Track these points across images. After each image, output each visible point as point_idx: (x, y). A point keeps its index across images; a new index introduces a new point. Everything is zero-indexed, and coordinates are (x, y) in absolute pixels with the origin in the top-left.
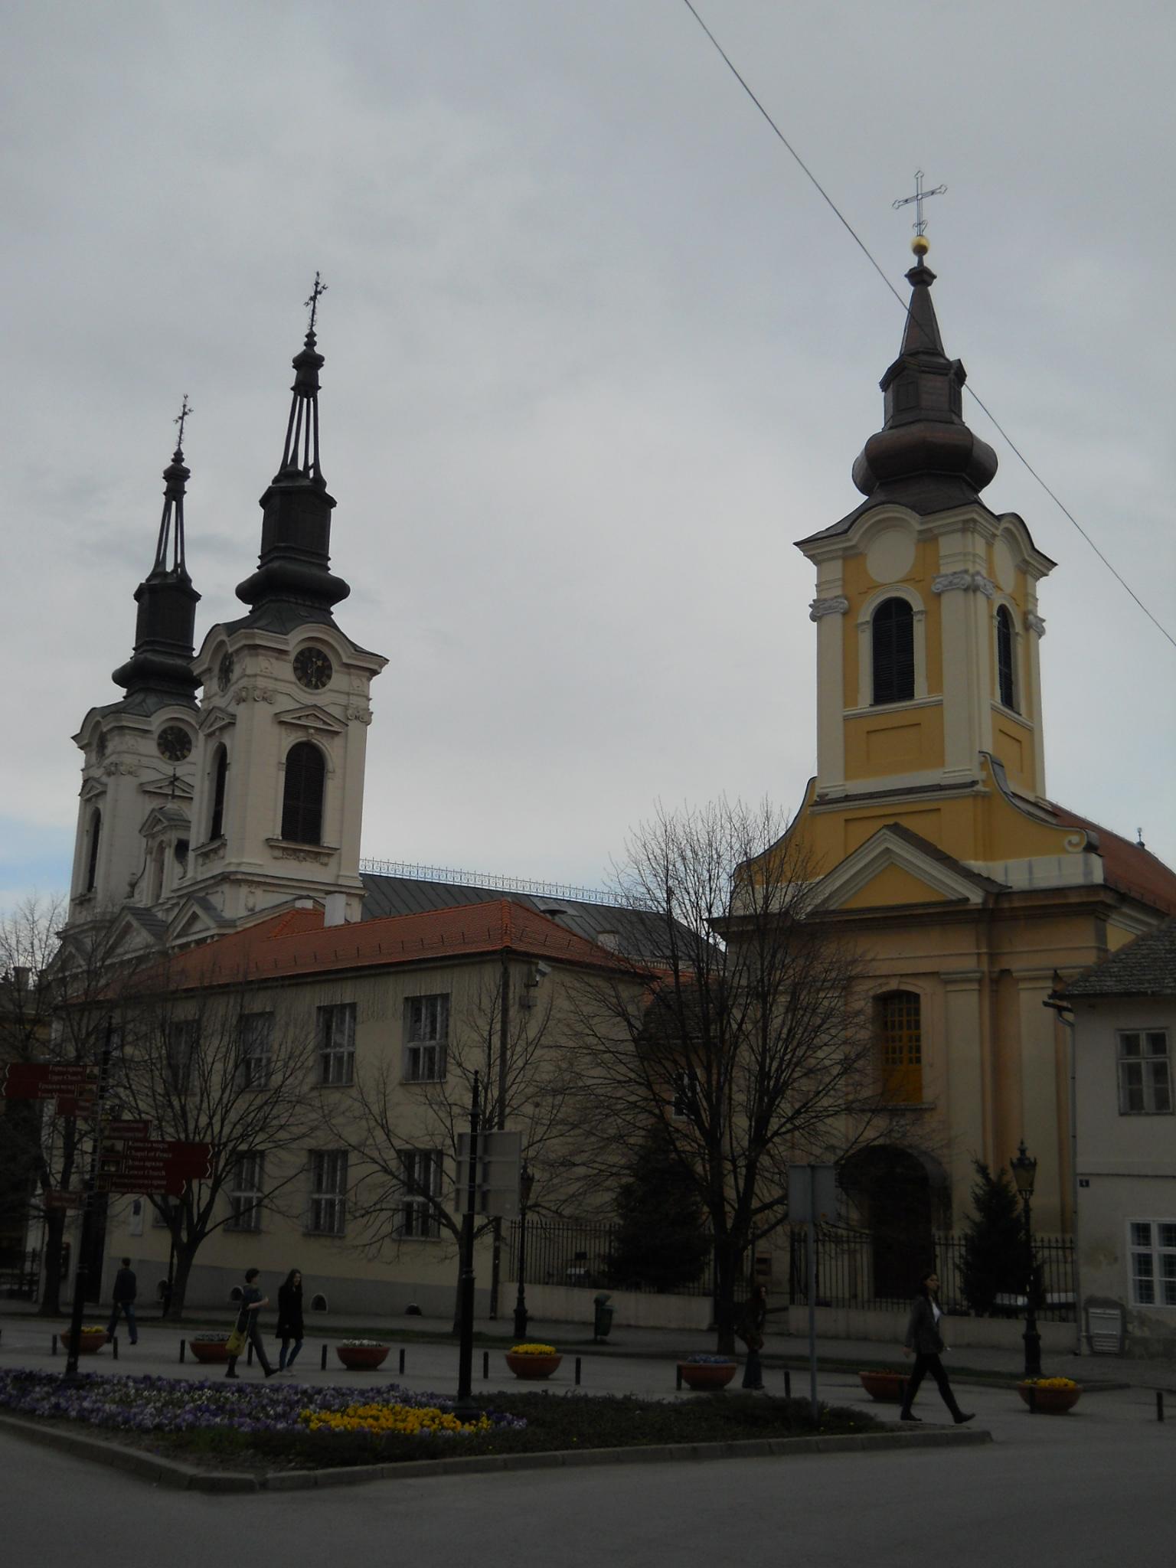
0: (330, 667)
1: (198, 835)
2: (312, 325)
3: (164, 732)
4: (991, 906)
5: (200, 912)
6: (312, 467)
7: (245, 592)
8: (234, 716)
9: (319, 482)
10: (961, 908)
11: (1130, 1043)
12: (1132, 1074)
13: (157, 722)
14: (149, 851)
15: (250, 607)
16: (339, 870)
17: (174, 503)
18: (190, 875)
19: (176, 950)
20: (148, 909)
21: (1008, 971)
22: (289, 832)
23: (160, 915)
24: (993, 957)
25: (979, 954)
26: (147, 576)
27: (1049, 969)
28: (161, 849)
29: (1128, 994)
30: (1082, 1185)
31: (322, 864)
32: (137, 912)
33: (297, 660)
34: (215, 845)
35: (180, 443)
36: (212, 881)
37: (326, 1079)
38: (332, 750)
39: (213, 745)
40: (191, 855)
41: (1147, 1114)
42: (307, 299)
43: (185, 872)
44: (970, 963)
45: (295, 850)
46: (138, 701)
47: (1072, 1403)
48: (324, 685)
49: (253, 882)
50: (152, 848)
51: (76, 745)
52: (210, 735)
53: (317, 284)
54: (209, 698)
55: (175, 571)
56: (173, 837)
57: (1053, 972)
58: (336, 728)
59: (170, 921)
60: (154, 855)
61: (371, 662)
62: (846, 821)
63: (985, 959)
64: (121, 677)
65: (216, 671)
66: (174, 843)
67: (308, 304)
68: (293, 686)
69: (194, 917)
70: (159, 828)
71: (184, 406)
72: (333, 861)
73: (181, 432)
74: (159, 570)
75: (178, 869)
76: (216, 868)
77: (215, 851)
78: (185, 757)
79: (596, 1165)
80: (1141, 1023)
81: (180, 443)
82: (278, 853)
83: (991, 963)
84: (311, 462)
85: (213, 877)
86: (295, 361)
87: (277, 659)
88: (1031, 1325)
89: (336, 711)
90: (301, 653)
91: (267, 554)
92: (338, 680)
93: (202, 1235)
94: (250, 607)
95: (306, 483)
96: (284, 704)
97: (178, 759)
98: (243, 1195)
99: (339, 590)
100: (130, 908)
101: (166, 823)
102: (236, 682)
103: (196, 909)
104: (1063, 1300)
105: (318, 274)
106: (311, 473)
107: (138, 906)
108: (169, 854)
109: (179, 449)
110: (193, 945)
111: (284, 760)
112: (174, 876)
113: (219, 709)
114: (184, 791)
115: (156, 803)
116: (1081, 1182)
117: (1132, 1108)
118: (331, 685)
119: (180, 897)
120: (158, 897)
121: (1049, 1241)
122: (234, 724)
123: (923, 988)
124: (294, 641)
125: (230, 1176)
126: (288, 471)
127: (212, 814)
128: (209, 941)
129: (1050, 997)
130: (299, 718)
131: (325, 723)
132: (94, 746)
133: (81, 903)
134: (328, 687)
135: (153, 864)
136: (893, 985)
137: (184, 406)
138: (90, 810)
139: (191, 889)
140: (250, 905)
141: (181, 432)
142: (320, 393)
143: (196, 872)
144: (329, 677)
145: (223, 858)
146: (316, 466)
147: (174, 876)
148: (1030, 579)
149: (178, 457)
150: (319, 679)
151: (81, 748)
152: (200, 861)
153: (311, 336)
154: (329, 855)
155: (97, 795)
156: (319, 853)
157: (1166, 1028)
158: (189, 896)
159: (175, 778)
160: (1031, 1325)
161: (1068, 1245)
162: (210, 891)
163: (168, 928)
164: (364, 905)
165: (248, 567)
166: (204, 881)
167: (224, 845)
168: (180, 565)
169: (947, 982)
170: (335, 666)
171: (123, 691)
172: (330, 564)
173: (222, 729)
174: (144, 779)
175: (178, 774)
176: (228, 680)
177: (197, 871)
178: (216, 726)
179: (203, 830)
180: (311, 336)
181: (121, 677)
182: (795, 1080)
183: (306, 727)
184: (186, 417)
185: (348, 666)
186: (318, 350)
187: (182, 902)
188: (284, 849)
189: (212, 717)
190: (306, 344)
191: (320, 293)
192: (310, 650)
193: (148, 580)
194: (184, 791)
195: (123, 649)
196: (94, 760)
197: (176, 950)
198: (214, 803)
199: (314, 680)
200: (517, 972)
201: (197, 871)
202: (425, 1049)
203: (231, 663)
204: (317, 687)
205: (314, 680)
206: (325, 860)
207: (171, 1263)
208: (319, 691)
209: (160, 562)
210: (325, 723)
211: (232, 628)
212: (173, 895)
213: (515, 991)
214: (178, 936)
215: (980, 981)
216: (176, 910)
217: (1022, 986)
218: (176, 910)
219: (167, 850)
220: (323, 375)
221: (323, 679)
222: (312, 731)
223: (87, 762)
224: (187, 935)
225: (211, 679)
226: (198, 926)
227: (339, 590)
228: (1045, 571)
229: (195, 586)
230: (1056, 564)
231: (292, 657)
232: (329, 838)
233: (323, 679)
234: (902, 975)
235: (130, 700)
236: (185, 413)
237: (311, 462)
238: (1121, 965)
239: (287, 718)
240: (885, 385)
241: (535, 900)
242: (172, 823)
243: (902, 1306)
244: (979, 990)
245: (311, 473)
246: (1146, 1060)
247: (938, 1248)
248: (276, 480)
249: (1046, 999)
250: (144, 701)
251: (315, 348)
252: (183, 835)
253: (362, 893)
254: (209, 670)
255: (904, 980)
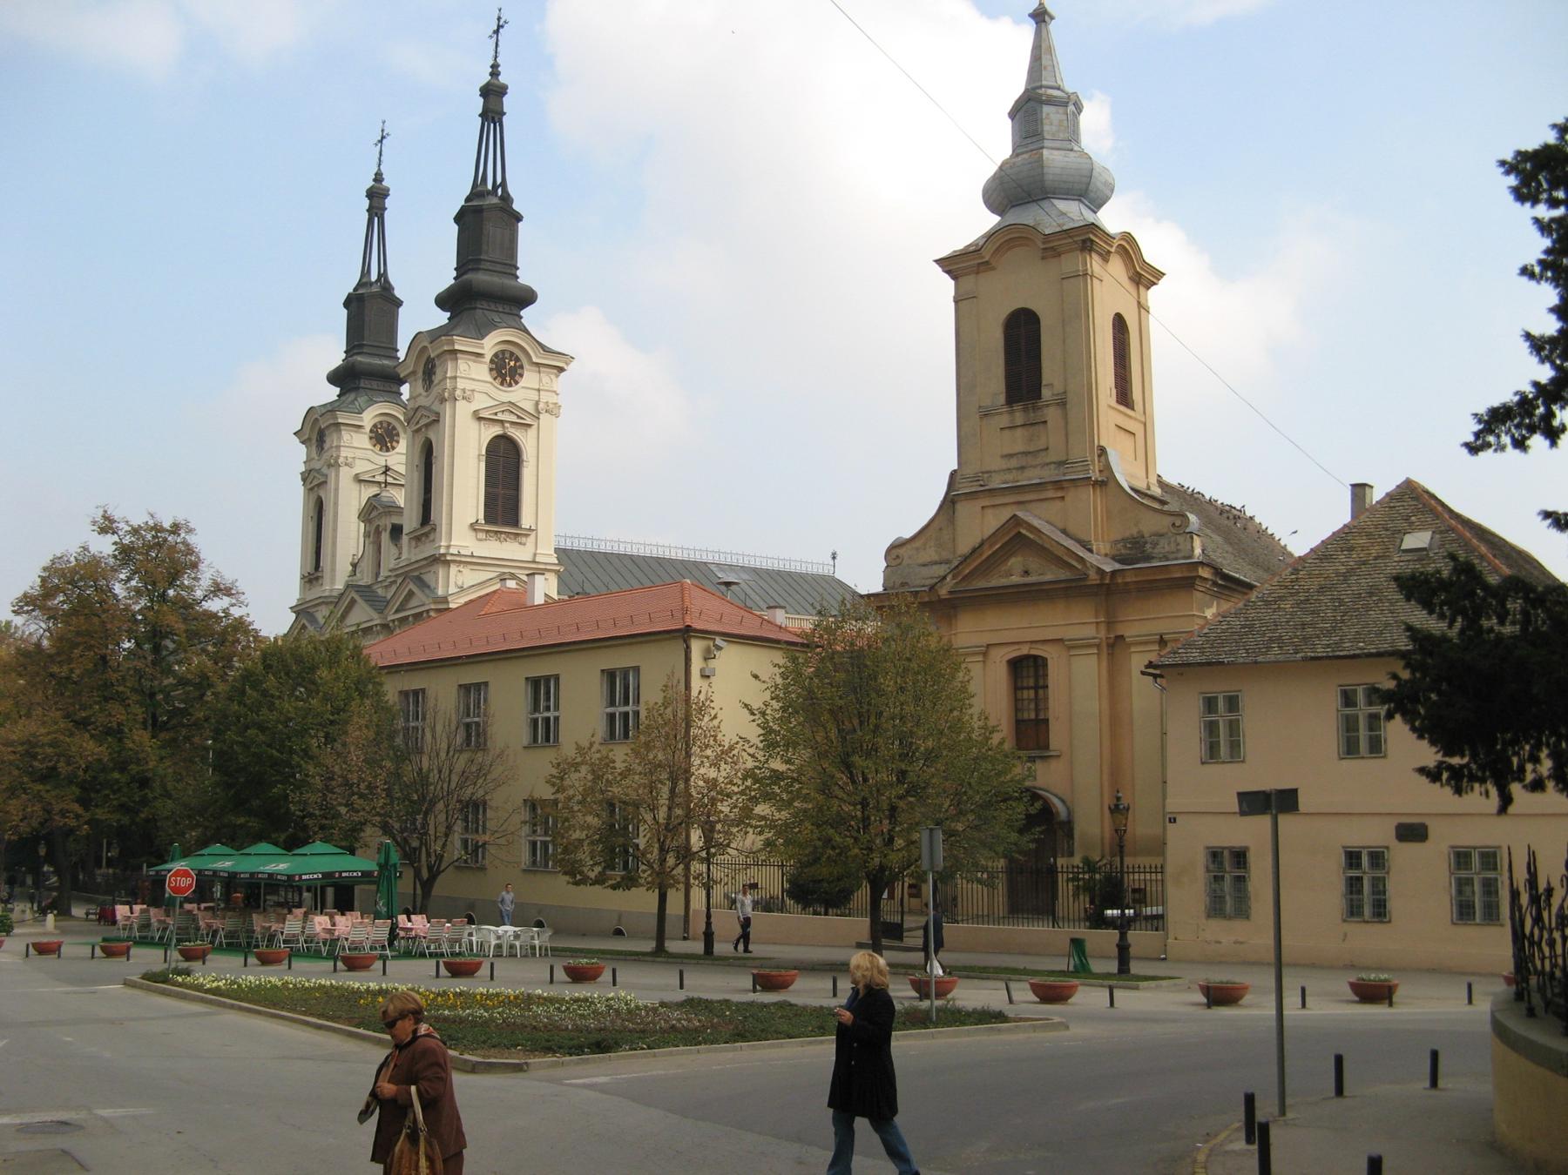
0: (522, 367)
1: (410, 522)
2: (496, 57)
3: (375, 426)
4: (1107, 581)
5: (415, 589)
6: (500, 185)
7: (443, 301)
8: (438, 414)
9: (507, 198)
10: (1082, 583)
11: (1210, 704)
12: (1212, 728)
13: (369, 417)
14: (367, 535)
15: (448, 314)
16: (536, 549)
17: (376, 219)
18: (404, 557)
19: (396, 623)
20: (369, 586)
21: (1122, 637)
22: (491, 516)
23: (380, 592)
24: (1110, 624)
25: (1097, 623)
26: (354, 286)
27: (1156, 634)
28: (378, 532)
29: (1209, 664)
30: (1170, 822)
31: (520, 543)
32: (360, 589)
33: (492, 361)
34: (427, 529)
35: (379, 165)
36: (424, 562)
37: (535, 739)
38: (526, 440)
39: (420, 440)
40: (405, 539)
41: (1224, 762)
42: (491, 33)
43: (400, 553)
44: (1089, 631)
45: (496, 532)
46: (350, 399)
47: (1241, 997)
48: (517, 383)
49: (461, 562)
50: (369, 532)
51: (298, 440)
52: (417, 431)
53: (499, 19)
54: (415, 398)
55: (379, 279)
56: (387, 522)
57: (1158, 637)
58: (528, 421)
59: (389, 597)
60: (371, 539)
61: (560, 361)
62: (983, 507)
63: (1103, 627)
64: (335, 378)
65: (420, 374)
66: (389, 527)
67: (491, 37)
68: (489, 385)
69: (411, 594)
70: (374, 513)
71: (383, 131)
72: (530, 540)
73: (381, 155)
74: (364, 280)
75: (394, 551)
76: (426, 551)
77: (426, 535)
78: (393, 448)
79: (1536, 932)
80: (1219, 687)
81: (379, 165)
82: (482, 535)
83: (1108, 630)
84: (499, 181)
85: (425, 559)
86: (481, 90)
87: (475, 362)
88: (1123, 936)
89: (529, 407)
90: (496, 355)
91: (461, 269)
92: (529, 378)
93: (439, 873)
94: (448, 314)
95: (495, 200)
96: (481, 402)
97: (388, 450)
98: (470, 837)
99: (526, 298)
100: (353, 586)
101: (381, 510)
102: (439, 383)
103: (412, 586)
104: (1154, 913)
105: (500, 10)
106: (500, 191)
107: (360, 583)
108: (385, 537)
109: (379, 169)
110: (411, 619)
111: (484, 452)
112: (391, 558)
113: (425, 408)
114: (395, 479)
115: (374, 490)
116: (1170, 819)
117: (1211, 758)
118: (523, 382)
119: (397, 576)
120: (377, 574)
121: (1156, 867)
122: (438, 421)
123: (1050, 653)
124: (490, 344)
125: (459, 822)
126: (477, 192)
127: (422, 501)
128: (425, 615)
129: (1147, 667)
130: (496, 414)
131: (519, 417)
132: (314, 441)
133: (310, 581)
134: (520, 384)
135: (371, 546)
136: (1025, 650)
137: (383, 131)
138: (313, 498)
139: (407, 569)
140: (460, 583)
141: (381, 155)
142: (505, 119)
143: (409, 552)
144: (521, 376)
145: (434, 540)
146: (504, 184)
147: (391, 558)
148: (1142, 289)
149: (378, 178)
150: (512, 378)
151: (303, 443)
152: (413, 543)
153: (495, 66)
154: (527, 536)
155: (319, 485)
156: (517, 535)
157: (1240, 691)
158: (406, 575)
159: (387, 469)
160: (1123, 936)
161: (1148, 870)
162: (422, 571)
163: (388, 602)
164: (560, 578)
165: (446, 278)
166: (417, 561)
167: (434, 530)
168: (383, 275)
169: (1070, 648)
170: (526, 365)
171: (337, 390)
172: (518, 273)
173: (427, 426)
174: (357, 469)
175: (389, 464)
176: (431, 382)
177: (411, 553)
178: (423, 422)
179: (414, 519)
180: (495, 66)
181: (335, 378)
182: (440, 858)
183: (502, 422)
184: (384, 141)
185: (538, 364)
186: (502, 79)
187: (399, 581)
188: (487, 531)
189: (418, 415)
190: (491, 74)
191: (502, 27)
192: (503, 352)
193: (355, 289)
194: (395, 479)
195: (335, 355)
196: (314, 455)
197: (396, 623)
198: (423, 492)
199: (508, 379)
200: (697, 647)
201: (411, 553)
202: (620, 713)
203: (434, 366)
204: (510, 385)
205: (508, 379)
206: (524, 539)
207: (415, 894)
208: (510, 389)
209: (365, 271)
210: (519, 417)
211: (436, 334)
212: (390, 574)
213: (697, 663)
214: (397, 611)
215: (1098, 646)
216: (394, 588)
217: (1133, 649)
218: (394, 588)
219: (383, 533)
220: (508, 102)
221: (495, 372)
222: (507, 425)
223: (308, 455)
224: (405, 610)
225: (416, 380)
226: (414, 602)
227: (526, 298)
228: (1155, 281)
229: (398, 293)
230: (1164, 274)
231: (488, 358)
232: (526, 520)
233: (495, 372)
234: (1032, 642)
235: (343, 398)
236: (383, 137)
237: (499, 181)
238: (1204, 639)
239: (482, 415)
240: (1013, 114)
241: (712, 567)
242: (387, 510)
243: (1011, 920)
244: (1098, 654)
245: (500, 191)
246: (1222, 717)
247: (1060, 875)
248: (468, 199)
249: (1144, 670)
250: (356, 399)
251: (500, 78)
252: (396, 520)
253: (558, 568)
254: (414, 373)
255: (1034, 646)
